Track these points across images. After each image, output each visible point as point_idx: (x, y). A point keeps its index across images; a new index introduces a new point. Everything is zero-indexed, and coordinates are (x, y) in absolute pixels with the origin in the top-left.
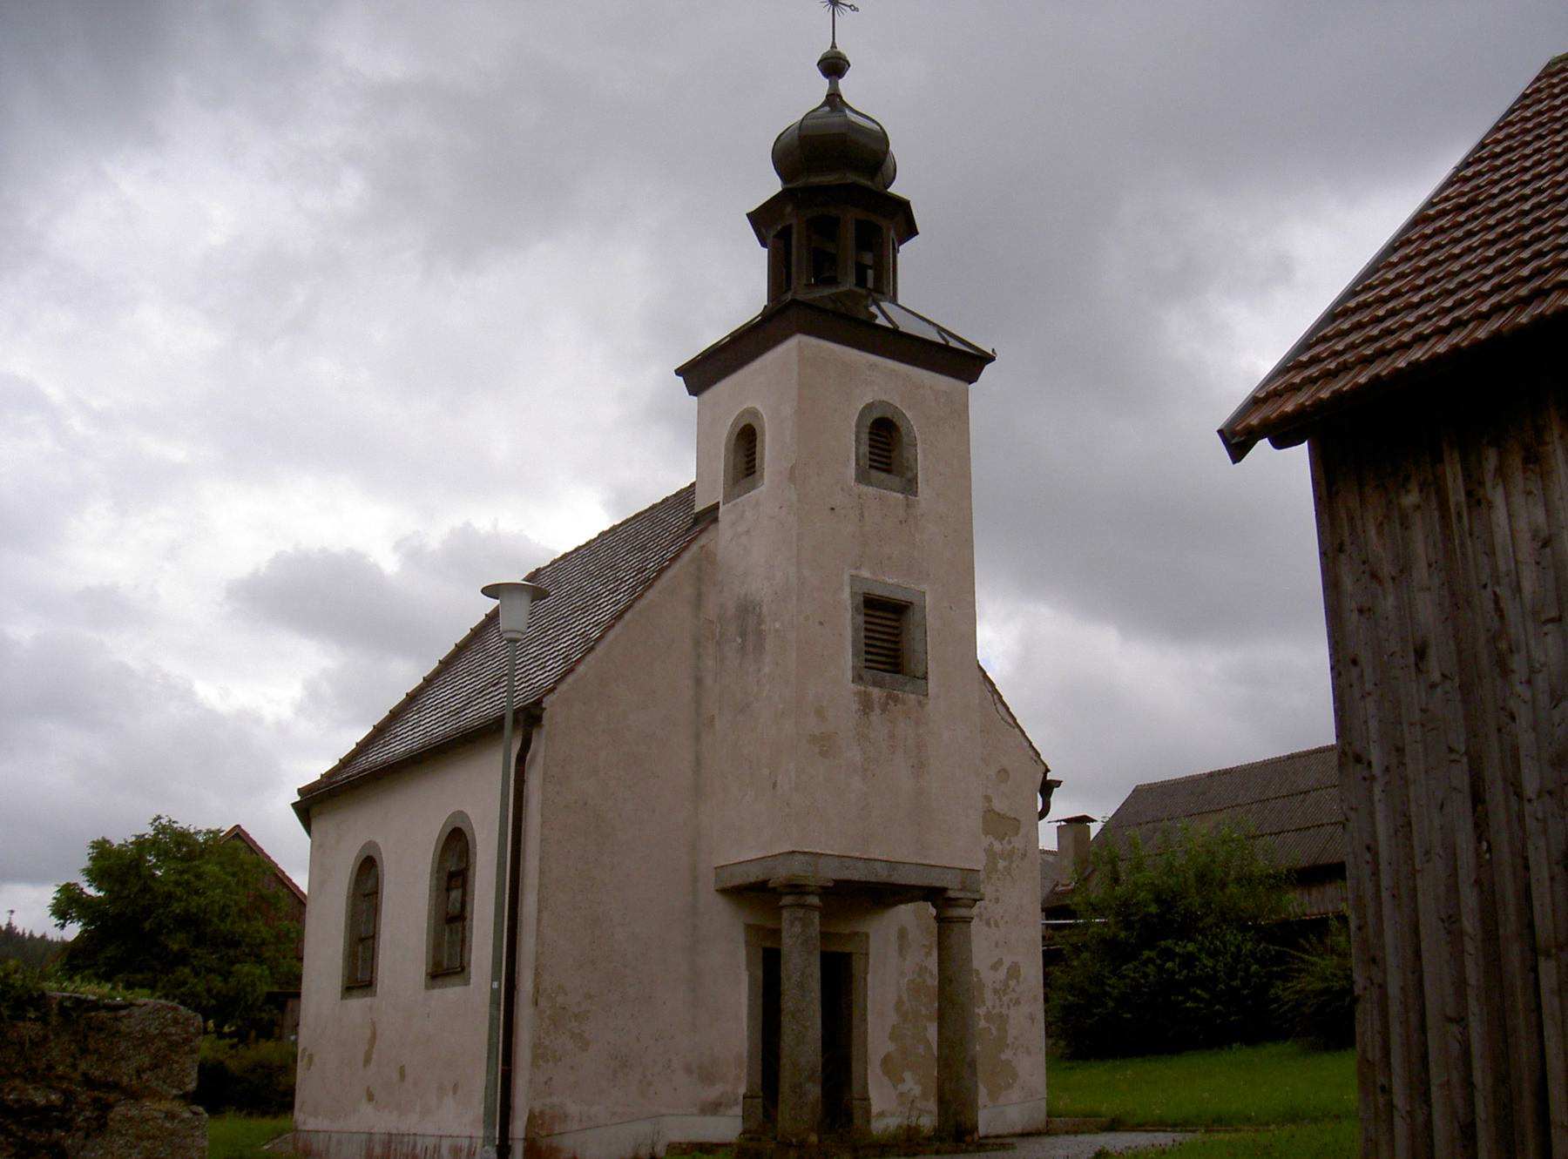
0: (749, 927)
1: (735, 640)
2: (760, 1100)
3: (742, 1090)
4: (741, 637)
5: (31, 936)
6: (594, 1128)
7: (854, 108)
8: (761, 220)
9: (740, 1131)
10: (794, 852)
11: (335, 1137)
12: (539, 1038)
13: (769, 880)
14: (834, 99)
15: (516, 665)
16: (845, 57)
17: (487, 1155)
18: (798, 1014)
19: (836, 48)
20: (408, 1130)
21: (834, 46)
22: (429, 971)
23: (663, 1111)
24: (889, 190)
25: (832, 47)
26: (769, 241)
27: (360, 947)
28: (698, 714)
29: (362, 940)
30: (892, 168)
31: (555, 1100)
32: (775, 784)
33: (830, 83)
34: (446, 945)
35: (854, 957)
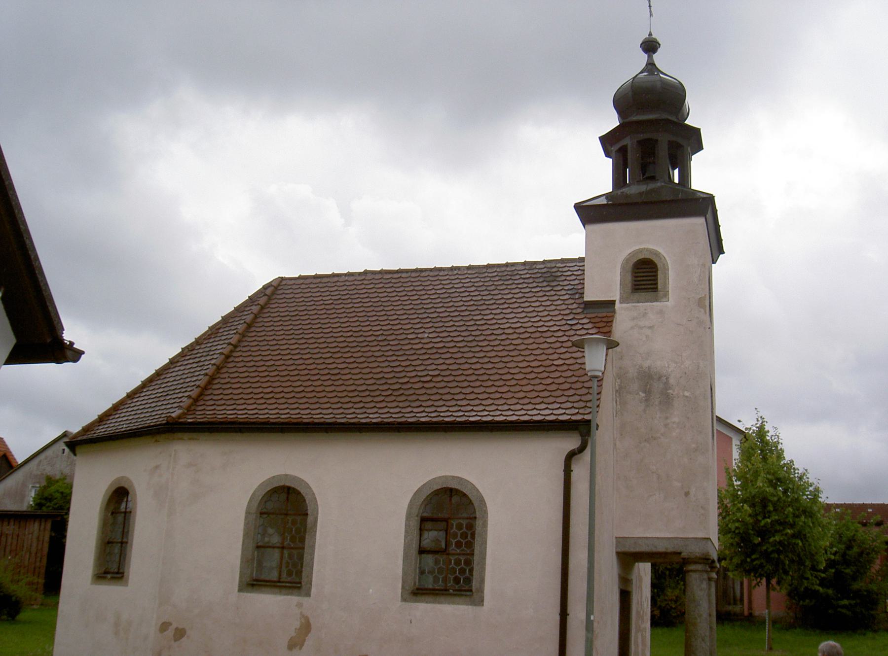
1: (638, 394)
4: (645, 392)
5: (817, 492)
6: (120, 564)
7: (711, 259)
8: (607, 141)
14: (651, 67)
16: (656, 40)
19: (652, 35)
21: (650, 34)
24: (686, 122)
25: (649, 35)
26: (613, 154)
30: (686, 114)
32: (687, 494)
33: (648, 57)
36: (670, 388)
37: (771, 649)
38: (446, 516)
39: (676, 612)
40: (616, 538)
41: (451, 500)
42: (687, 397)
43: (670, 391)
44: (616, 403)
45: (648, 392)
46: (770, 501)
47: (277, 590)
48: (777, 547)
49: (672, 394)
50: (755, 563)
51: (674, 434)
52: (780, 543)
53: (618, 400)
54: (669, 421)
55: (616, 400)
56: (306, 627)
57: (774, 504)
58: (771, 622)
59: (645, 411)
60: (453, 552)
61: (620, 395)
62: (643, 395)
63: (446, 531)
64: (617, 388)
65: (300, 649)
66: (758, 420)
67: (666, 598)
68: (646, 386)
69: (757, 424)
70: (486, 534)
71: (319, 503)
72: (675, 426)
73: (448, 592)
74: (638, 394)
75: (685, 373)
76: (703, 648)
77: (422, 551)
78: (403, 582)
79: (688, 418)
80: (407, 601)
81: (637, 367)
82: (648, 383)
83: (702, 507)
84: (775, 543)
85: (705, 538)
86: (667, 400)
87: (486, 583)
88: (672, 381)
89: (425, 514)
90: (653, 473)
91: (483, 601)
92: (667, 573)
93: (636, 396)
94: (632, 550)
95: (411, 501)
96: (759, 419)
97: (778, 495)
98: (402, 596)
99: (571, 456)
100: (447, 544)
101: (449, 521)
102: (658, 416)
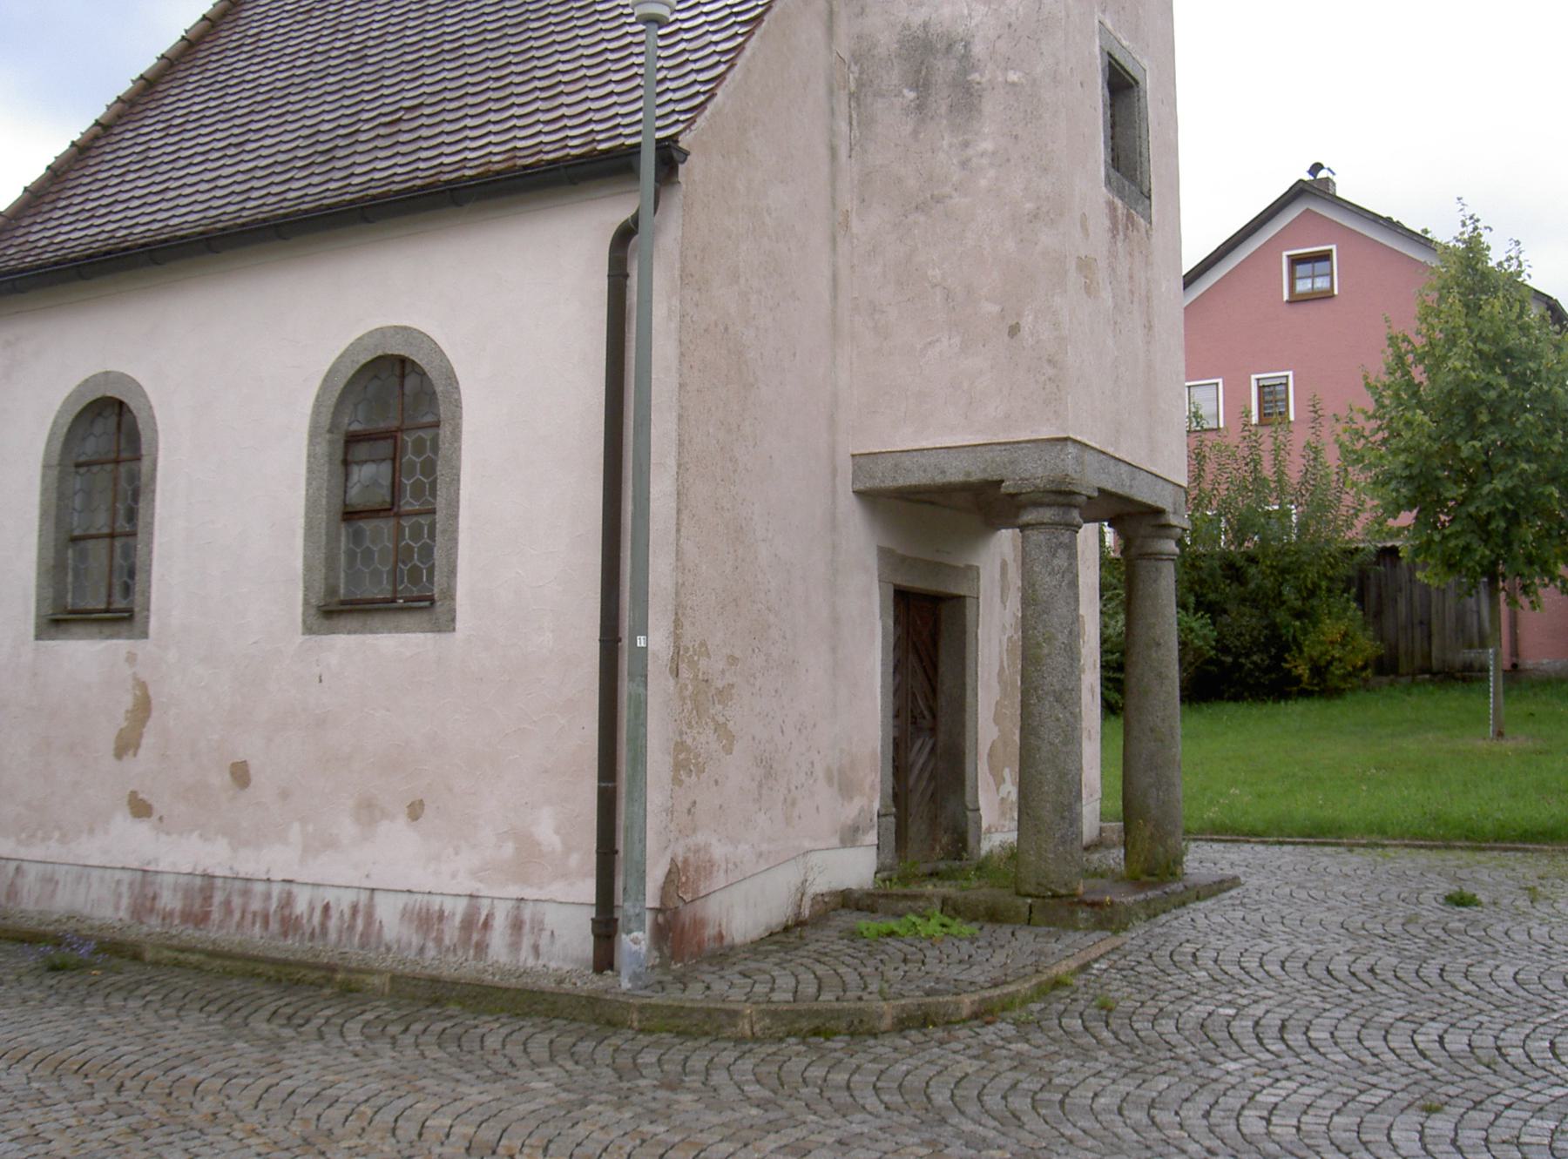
0: (884, 553)
1: (899, 94)
2: (892, 819)
3: (876, 806)
4: (915, 87)
9: (874, 869)
10: (1066, 439)
11: (32, 872)
12: (681, 733)
13: (1002, 481)
15: (659, 58)
17: (635, 948)
18: (1067, 696)
20: (268, 871)
22: (314, 601)
23: (807, 844)
27: (70, 553)
28: (834, 205)
29: (75, 540)
31: (700, 838)
32: (1014, 330)
34: (343, 558)
35: (968, 600)
36: (974, 68)
37: (1500, 734)
38: (393, 423)
39: (1344, 668)
40: (853, 456)
41: (402, 386)
42: (1014, 84)
43: (975, 76)
44: (851, 124)
45: (923, 86)
46: (1481, 402)
47: (94, 629)
48: (1501, 505)
49: (979, 83)
50: (1452, 544)
51: (983, 183)
52: (1509, 494)
53: (854, 116)
54: (970, 152)
55: (850, 117)
56: (143, 708)
57: (1493, 409)
58: (1501, 674)
59: (915, 133)
60: (408, 508)
61: (859, 105)
62: (911, 95)
63: (394, 460)
64: (853, 88)
65: (135, 755)
66: (1464, 224)
67: (1322, 638)
68: (919, 71)
69: (1462, 233)
70: (459, 458)
71: (160, 427)
72: (985, 161)
73: (394, 605)
74: (899, 94)
75: (1010, 25)
76: (1058, 720)
77: (350, 515)
78: (307, 589)
79: (1016, 137)
80: (314, 633)
81: (899, 28)
82: (922, 63)
83: (1049, 361)
84: (1494, 496)
85: (1058, 440)
86: (966, 99)
87: (459, 575)
88: (978, 49)
89: (356, 427)
90: (934, 286)
91: (453, 620)
92: (1324, 584)
93: (895, 100)
94: (889, 483)
95: (318, 397)
96: (1468, 222)
97: (1498, 385)
98: (304, 622)
99: (625, 236)
100: (395, 488)
101: (399, 435)
102: (945, 143)
